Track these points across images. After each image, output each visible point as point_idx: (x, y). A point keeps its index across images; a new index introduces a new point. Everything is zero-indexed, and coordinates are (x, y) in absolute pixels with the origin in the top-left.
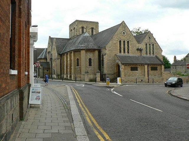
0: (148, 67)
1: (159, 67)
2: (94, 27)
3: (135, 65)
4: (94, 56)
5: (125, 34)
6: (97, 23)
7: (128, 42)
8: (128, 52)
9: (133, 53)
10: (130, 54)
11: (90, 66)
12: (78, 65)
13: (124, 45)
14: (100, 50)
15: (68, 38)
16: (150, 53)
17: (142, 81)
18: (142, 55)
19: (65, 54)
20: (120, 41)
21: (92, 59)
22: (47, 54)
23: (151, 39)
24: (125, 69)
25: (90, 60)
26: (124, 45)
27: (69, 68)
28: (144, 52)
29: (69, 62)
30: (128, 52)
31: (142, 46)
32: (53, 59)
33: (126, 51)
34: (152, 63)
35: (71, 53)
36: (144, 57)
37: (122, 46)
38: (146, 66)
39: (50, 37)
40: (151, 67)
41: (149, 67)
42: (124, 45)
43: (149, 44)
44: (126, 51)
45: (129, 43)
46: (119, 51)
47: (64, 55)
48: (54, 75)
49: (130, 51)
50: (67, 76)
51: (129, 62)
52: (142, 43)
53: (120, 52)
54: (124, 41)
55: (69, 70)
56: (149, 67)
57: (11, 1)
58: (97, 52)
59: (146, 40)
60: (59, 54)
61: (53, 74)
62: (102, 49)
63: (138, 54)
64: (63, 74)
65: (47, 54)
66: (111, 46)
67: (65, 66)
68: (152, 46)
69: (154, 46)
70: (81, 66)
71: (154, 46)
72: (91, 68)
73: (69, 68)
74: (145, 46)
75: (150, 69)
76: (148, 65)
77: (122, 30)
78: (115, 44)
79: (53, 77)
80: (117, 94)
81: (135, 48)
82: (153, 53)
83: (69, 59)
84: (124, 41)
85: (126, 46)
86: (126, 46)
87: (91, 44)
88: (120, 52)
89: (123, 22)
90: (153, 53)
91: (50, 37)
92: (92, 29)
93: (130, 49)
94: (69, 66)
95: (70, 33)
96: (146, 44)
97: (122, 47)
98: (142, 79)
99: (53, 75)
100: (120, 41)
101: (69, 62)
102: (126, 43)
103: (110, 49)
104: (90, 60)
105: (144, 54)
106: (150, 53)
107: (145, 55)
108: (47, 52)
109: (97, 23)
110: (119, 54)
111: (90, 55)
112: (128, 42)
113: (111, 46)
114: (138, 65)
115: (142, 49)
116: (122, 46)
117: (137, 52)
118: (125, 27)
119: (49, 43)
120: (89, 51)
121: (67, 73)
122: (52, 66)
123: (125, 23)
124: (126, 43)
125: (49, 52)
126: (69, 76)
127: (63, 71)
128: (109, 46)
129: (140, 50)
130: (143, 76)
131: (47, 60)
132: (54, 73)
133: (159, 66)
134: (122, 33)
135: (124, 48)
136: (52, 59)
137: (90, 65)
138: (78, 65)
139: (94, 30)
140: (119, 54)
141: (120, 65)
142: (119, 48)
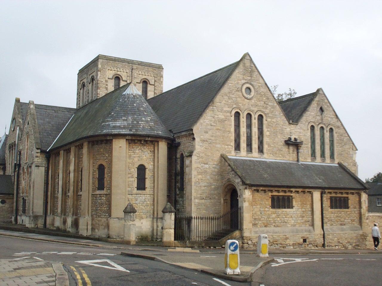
0: (322, 197)
1: (352, 199)
2: (149, 78)
3: (285, 192)
4: (155, 159)
5: (253, 93)
6: (160, 68)
7: (261, 117)
8: (261, 150)
9: (275, 154)
10: (265, 155)
11: (140, 192)
12: (101, 187)
13: (248, 127)
14: (173, 140)
15: (75, 107)
16: (323, 155)
17: (305, 241)
18: (300, 159)
19: (62, 152)
20: (237, 115)
21: (149, 166)
22: (7, 151)
23: (325, 113)
24: (253, 203)
25: (141, 169)
26: (249, 126)
27: (70, 194)
28: (305, 150)
29: (72, 175)
30: (261, 150)
31: (300, 131)
32: (22, 165)
33: (255, 145)
34: (333, 185)
35: (80, 147)
36: (307, 167)
37: (243, 129)
38: (317, 195)
39: (18, 101)
40: (331, 198)
41: (326, 197)
42: (249, 126)
43: (320, 126)
44: (255, 145)
45: (265, 122)
46: (233, 144)
47: (58, 154)
48: (24, 218)
49: (265, 147)
50: (65, 222)
51: (267, 178)
52: (300, 125)
53: (238, 147)
54: (249, 116)
55: (70, 202)
56: (324, 199)
57: (1, 229)
58: (163, 147)
59: (311, 115)
60: (42, 152)
61: (20, 212)
62: (179, 137)
63: (287, 157)
64: (53, 212)
65: (7, 151)
66: (209, 127)
67: (60, 190)
68: (327, 135)
69: (335, 135)
70: (110, 188)
71: (331, 134)
72: (143, 198)
73: (70, 194)
74: (309, 134)
75: (327, 203)
76: (323, 190)
77: (243, 81)
78: (222, 121)
79: (20, 221)
80: (103, 266)
81: (281, 139)
82: (332, 156)
83: (72, 168)
84: (249, 116)
85: (255, 130)
86: (255, 130)
87: (147, 122)
88: (238, 147)
89: (246, 56)
90: (332, 156)
91: (18, 101)
92: (145, 83)
93: (266, 140)
94: (72, 188)
95: (78, 94)
96: (312, 127)
97: (242, 133)
98: (305, 235)
99: (21, 216)
100: (237, 115)
101: (72, 175)
102: (255, 122)
103: (207, 136)
104: (141, 169)
105: (305, 158)
106: (323, 155)
107: (308, 161)
108: (7, 146)
109: (160, 68)
110: (232, 155)
111: (143, 155)
112: (261, 117)
113: (209, 127)
114: (293, 190)
115: (301, 143)
116: (243, 129)
117: (285, 149)
118: (252, 72)
119: (14, 119)
120: (140, 141)
121: (64, 212)
122: (18, 188)
123: (251, 60)
124: (255, 122)
125: (12, 146)
126: (69, 221)
127: (54, 206)
128: (202, 129)
129: (293, 144)
130: (308, 227)
131: (4, 169)
132: (24, 211)
133: (353, 194)
134: (244, 90)
135: (247, 137)
136: (19, 165)
137: (141, 186)
138: (101, 187)
139: (150, 88)
140: (233, 153)
141: (240, 187)
142: (232, 136)
